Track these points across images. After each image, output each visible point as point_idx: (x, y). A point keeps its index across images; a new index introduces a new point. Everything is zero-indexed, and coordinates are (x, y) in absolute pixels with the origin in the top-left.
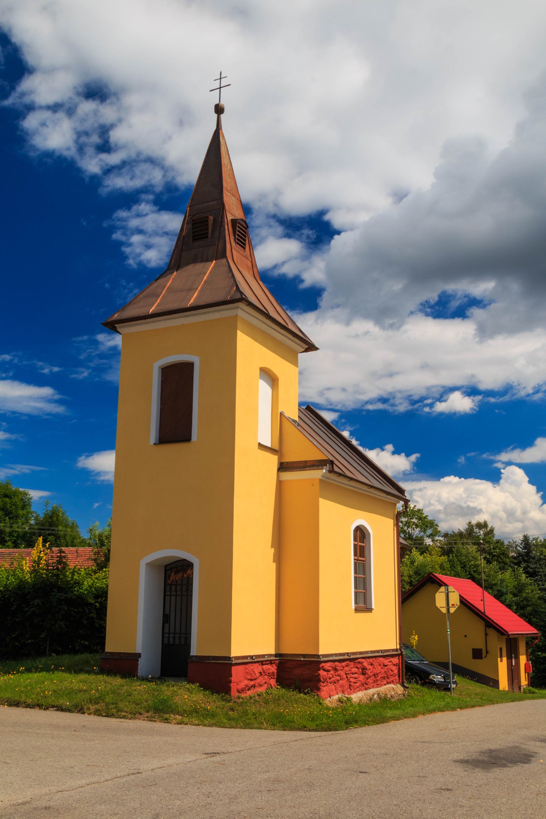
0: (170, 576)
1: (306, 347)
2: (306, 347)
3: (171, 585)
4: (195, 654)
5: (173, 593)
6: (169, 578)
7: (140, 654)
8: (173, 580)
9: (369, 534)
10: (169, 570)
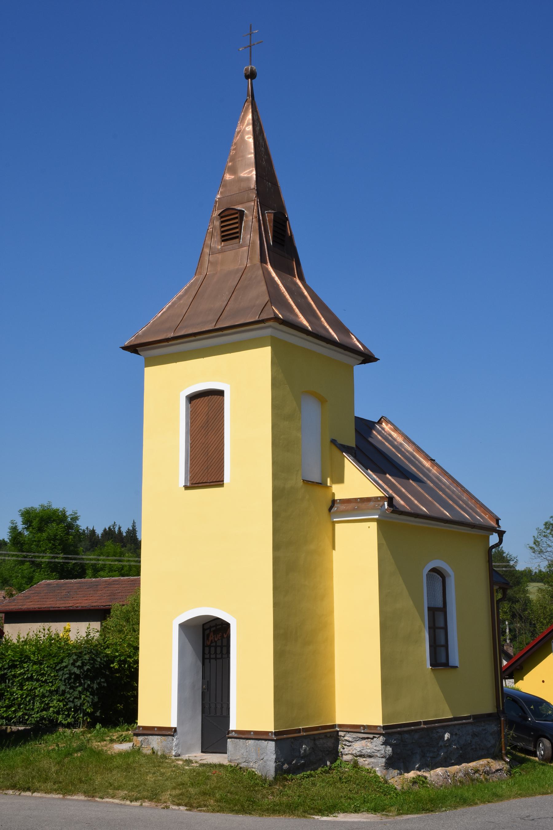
0: (208, 635)
1: (362, 359)
2: (362, 359)
3: (210, 646)
4: (235, 729)
5: (213, 656)
6: (208, 639)
7: (175, 729)
8: (212, 641)
9: (449, 576)
10: (207, 629)
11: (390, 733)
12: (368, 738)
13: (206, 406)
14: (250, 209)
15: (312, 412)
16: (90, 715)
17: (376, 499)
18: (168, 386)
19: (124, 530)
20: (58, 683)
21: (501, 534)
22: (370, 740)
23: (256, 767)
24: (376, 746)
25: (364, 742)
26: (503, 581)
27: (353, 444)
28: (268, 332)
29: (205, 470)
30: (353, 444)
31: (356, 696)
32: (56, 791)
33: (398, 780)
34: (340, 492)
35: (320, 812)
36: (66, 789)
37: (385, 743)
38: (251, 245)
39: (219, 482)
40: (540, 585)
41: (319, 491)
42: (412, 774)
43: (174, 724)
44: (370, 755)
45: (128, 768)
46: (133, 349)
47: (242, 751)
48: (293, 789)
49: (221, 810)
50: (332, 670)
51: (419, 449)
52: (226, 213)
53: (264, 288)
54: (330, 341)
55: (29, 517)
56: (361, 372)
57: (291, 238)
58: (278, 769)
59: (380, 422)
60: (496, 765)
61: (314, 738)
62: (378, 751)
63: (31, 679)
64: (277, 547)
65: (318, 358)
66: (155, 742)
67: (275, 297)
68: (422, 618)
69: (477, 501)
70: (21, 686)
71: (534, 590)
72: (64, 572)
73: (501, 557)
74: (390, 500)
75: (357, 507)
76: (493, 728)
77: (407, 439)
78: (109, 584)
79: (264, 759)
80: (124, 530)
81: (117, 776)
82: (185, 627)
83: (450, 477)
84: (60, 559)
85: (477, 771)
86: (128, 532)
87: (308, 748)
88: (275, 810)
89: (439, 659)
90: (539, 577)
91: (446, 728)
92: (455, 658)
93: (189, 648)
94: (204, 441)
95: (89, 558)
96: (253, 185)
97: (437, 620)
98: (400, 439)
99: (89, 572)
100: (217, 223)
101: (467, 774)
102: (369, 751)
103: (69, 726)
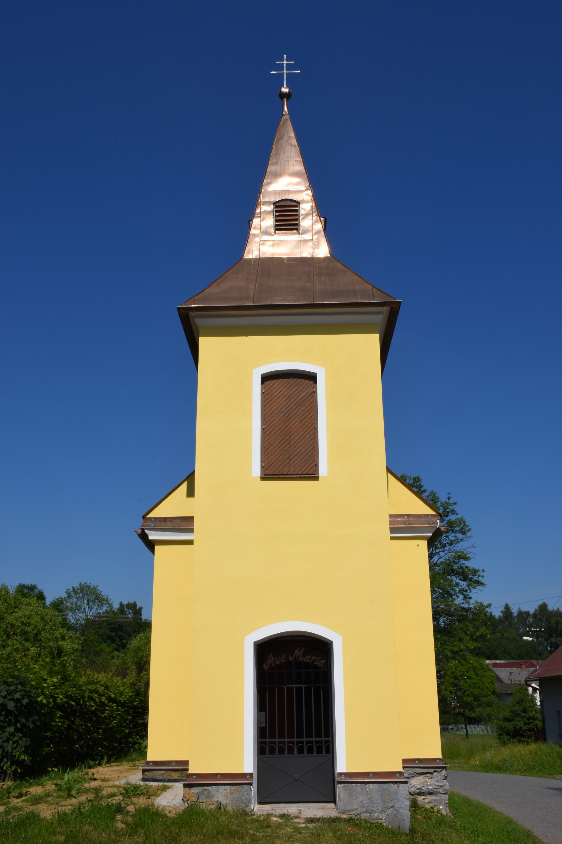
4: (345, 771)
12: (426, 773)
22: (429, 775)
25: (421, 778)
39: (312, 474)
47: (361, 798)
52: (283, 203)
62: (441, 786)
94: (283, 428)
102: (430, 787)
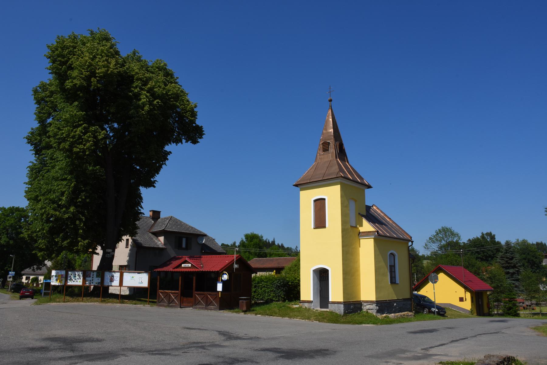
11: (378, 303)
13: (320, 204)
14: (332, 142)
15: (352, 204)
16: (283, 298)
17: (373, 232)
18: (307, 198)
19: (270, 241)
20: (273, 288)
21: (412, 242)
23: (338, 312)
24: (374, 306)
26: (414, 258)
27: (365, 214)
28: (339, 180)
29: (320, 222)
30: (365, 214)
31: (368, 292)
32: (280, 316)
33: (380, 316)
34: (362, 229)
35: (357, 324)
36: (283, 316)
37: (376, 306)
38: (333, 153)
39: (324, 226)
40: (429, 261)
41: (355, 229)
42: (384, 315)
43: (312, 300)
44: (372, 309)
45: (299, 311)
46: (296, 185)
48: (350, 317)
49: (329, 322)
50: (360, 284)
51: (381, 212)
53: (337, 167)
54: (358, 182)
55: (247, 236)
56: (367, 191)
57: (344, 150)
58: (344, 312)
59: (372, 206)
60: (410, 313)
61: (355, 304)
63: (264, 287)
64: (343, 246)
65: (354, 187)
66: (306, 305)
67: (341, 170)
68: (387, 267)
69: (405, 231)
70: (261, 289)
71: (425, 262)
72: (260, 255)
73: (413, 249)
74: (378, 232)
75: (367, 234)
76: (409, 302)
77: (381, 212)
78: (277, 260)
79: (340, 309)
80: (270, 241)
81: (296, 313)
82: (315, 271)
83: (396, 224)
84: (258, 251)
85: (404, 315)
86: (272, 242)
87: (353, 307)
88: (344, 323)
89: (393, 281)
90: (428, 258)
91: (395, 302)
92: (398, 281)
93: (316, 278)
95: (267, 251)
96: (332, 134)
97: (392, 269)
98: (379, 212)
99: (268, 256)
100: (321, 146)
101: (401, 316)
103: (277, 301)
